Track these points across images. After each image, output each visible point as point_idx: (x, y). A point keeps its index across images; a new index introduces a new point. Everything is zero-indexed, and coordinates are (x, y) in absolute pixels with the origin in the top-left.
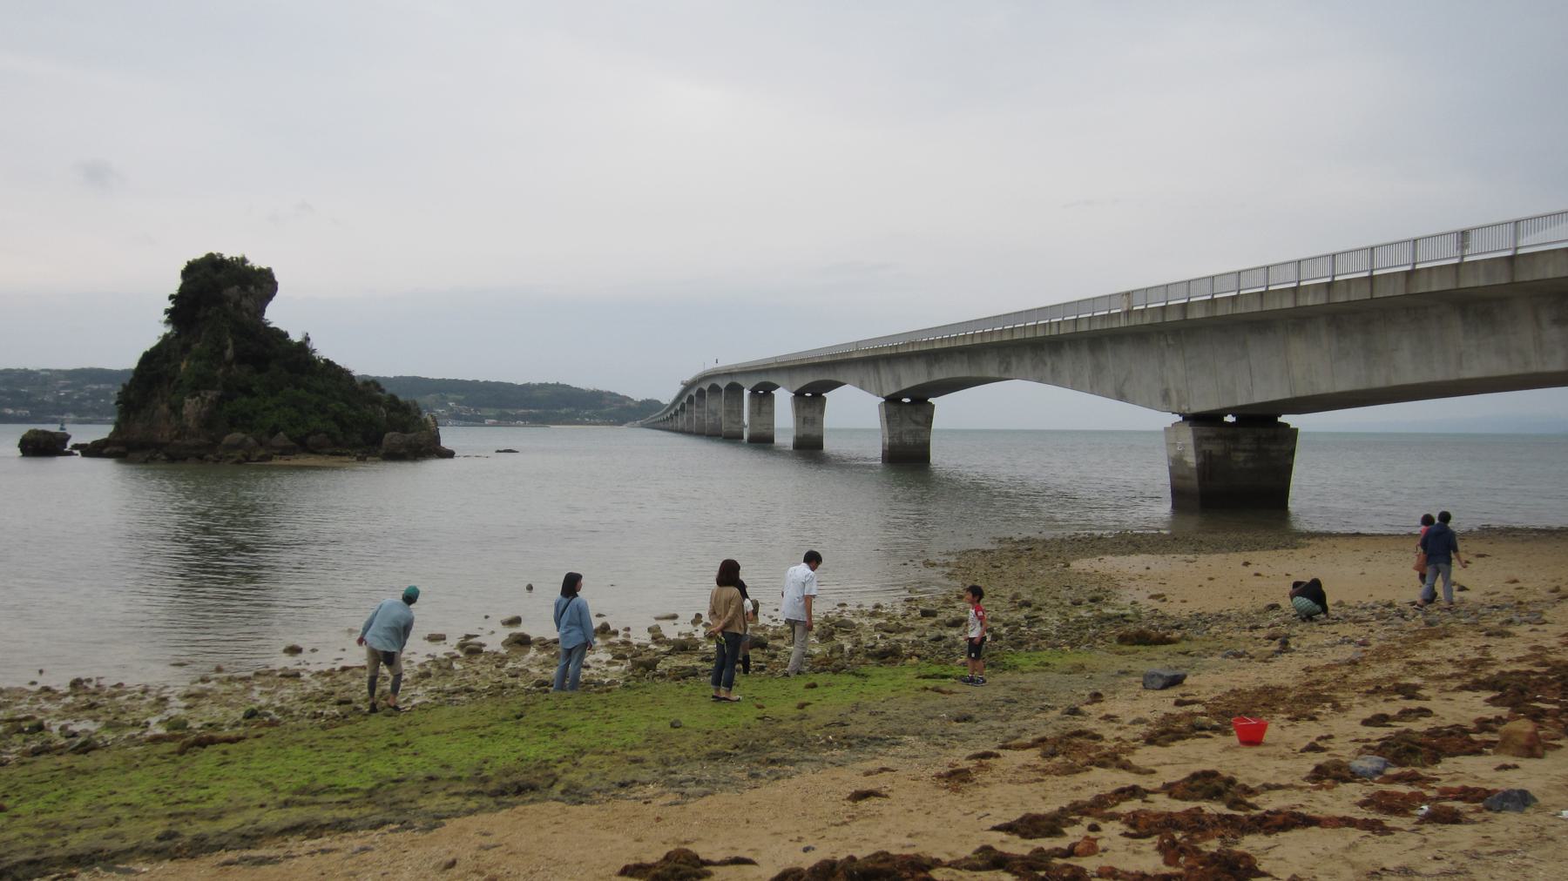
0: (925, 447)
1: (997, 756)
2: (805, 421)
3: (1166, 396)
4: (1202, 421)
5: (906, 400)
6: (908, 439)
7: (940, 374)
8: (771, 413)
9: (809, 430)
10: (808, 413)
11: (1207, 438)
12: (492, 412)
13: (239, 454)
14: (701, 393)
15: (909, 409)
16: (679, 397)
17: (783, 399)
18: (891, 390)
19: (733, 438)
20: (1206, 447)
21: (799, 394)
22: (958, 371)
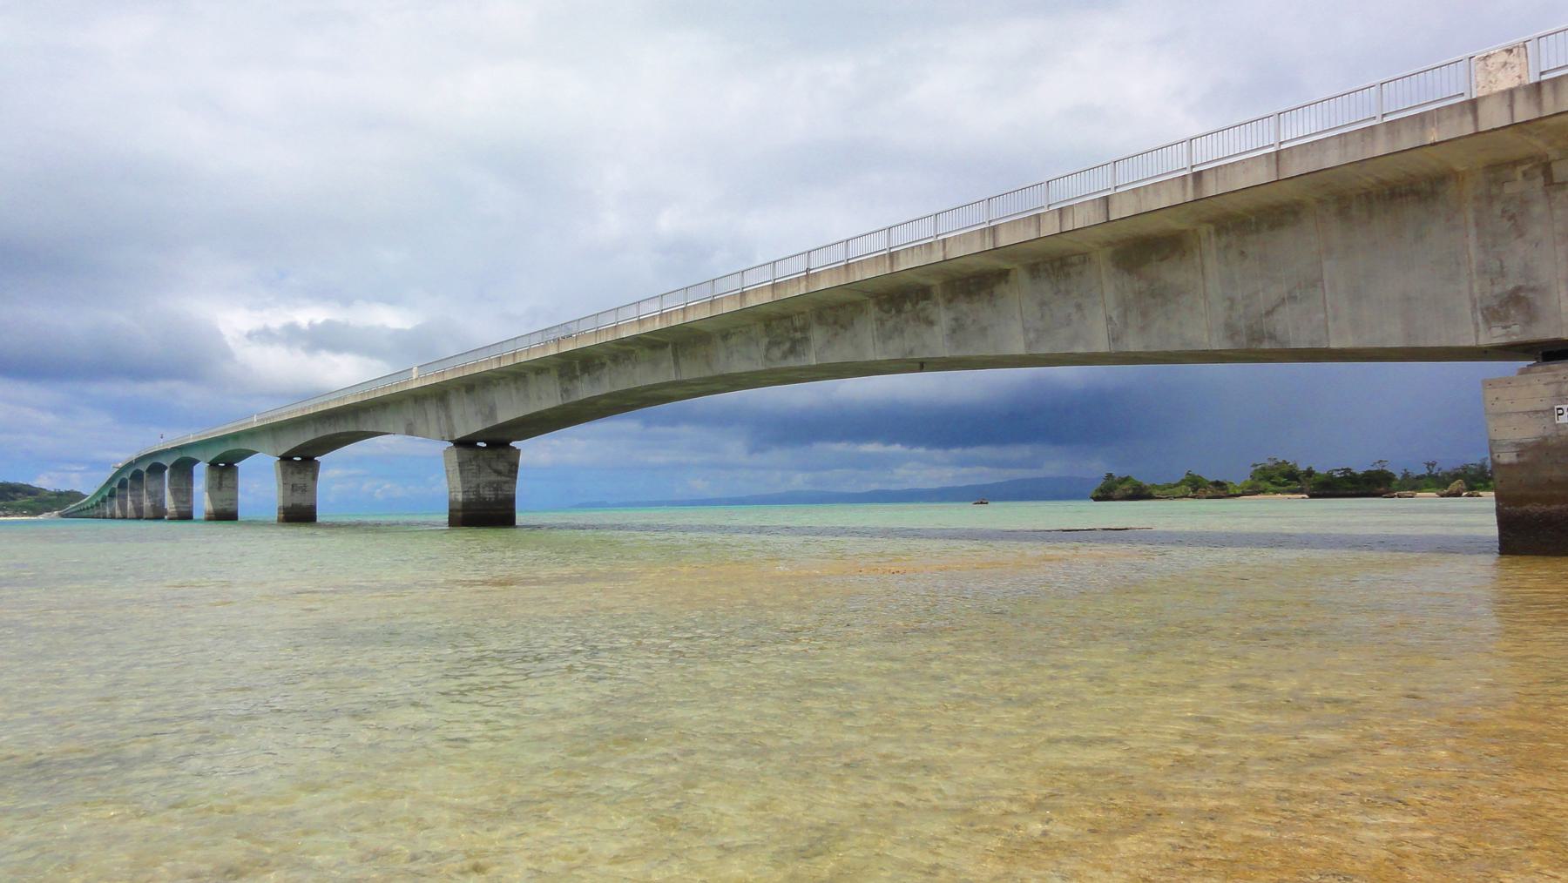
0: (510, 501)
1: (475, 816)
2: (294, 488)
6: (488, 494)
8: (235, 488)
9: (298, 499)
10: (297, 479)
15: (490, 450)
16: (100, 492)
17: (201, 471)
22: (351, 427)
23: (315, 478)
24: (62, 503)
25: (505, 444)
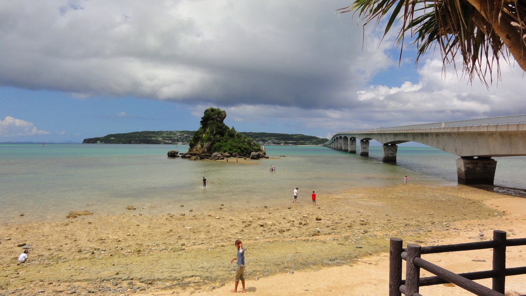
2: (364, 148)
3: (456, 151)
4: (467, 159)
5: (390, 145)
6: (390, 155)
7: (397, 139)
9: (365, 151)
10: (364, 146)
11: (468, 163)
12: (283, 141)
13: (216, 158)
14: (337, 138)
16: (332, 139)
17: (358, 141)
18: (385, 142)
19: (346, 151)
20: (468, 166)
21: (362, 141)
23: (368, 145)
24: (323, 141)
25: (395, 145)
